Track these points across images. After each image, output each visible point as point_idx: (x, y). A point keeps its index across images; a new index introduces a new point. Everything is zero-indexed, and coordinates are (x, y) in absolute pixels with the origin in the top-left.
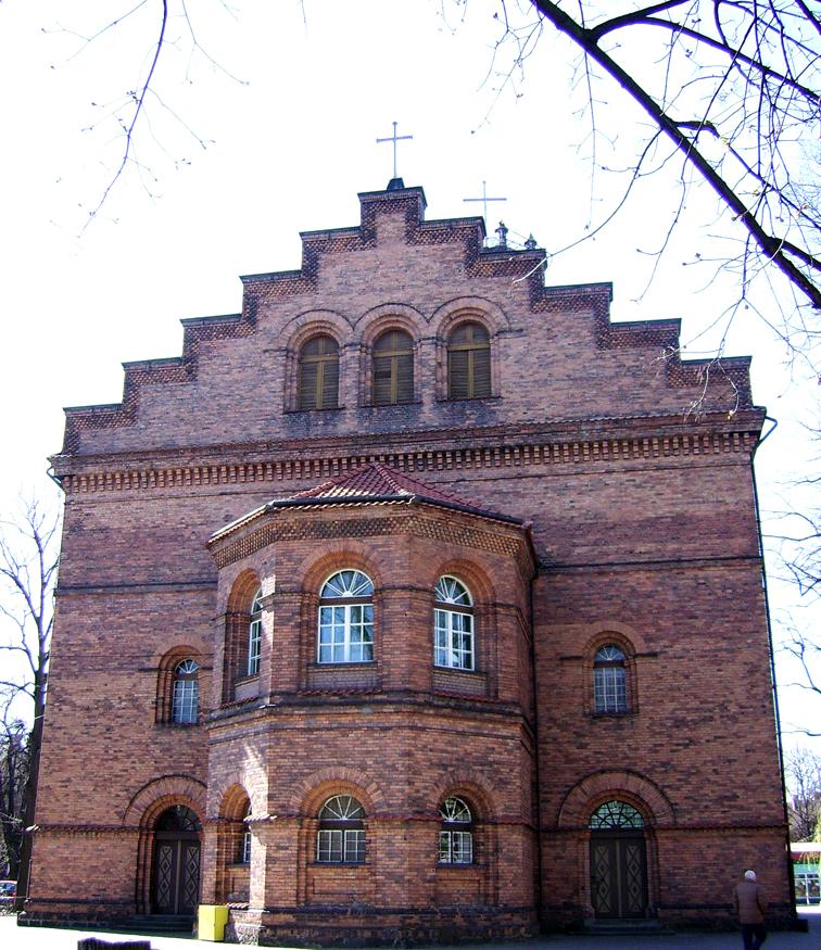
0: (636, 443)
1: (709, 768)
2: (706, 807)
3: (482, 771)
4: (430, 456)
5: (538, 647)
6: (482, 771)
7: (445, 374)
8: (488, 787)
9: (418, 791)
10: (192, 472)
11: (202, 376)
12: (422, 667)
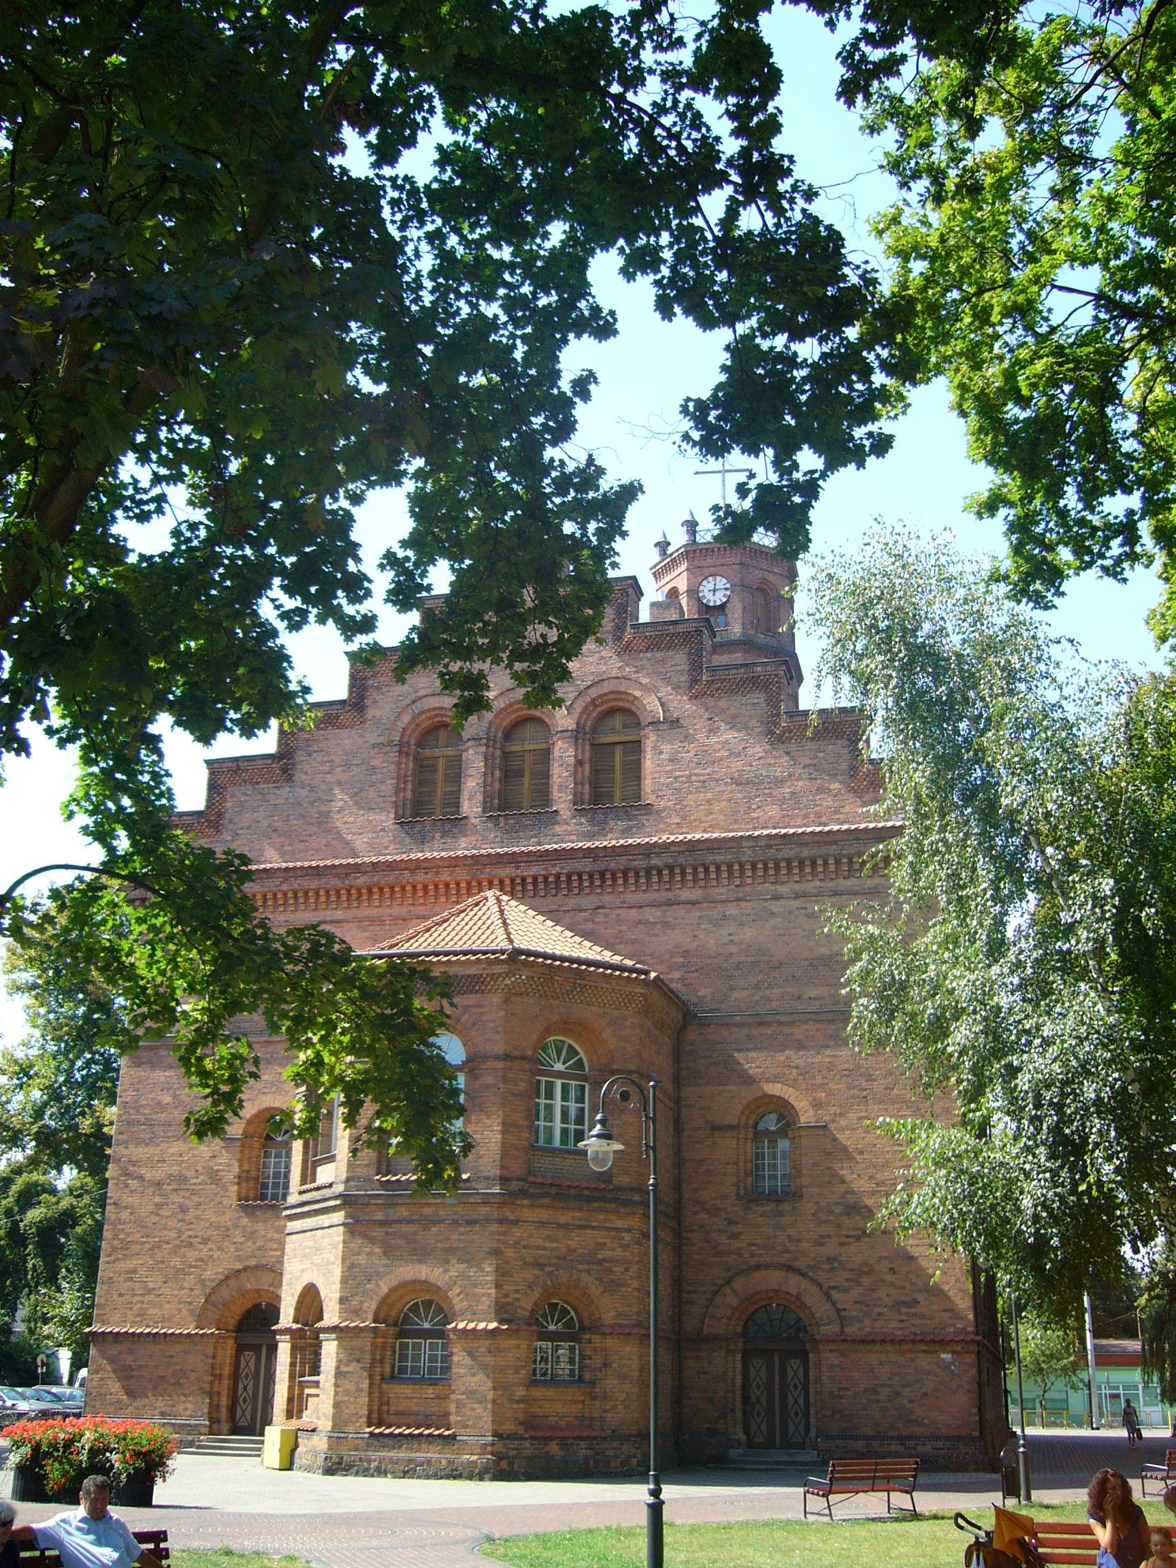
0: (808, 862)
1: (885, 1266)
2: (880, 1314)
3: (588, 1271)
4: (563, 878)
5: (685, 1114)
6: (588, 1271)
7: (587, 773)
8: (595, 1291)
9: (506, 1296)
10: (285, 895)
11: (299, 777)
12: (517, 1149)
